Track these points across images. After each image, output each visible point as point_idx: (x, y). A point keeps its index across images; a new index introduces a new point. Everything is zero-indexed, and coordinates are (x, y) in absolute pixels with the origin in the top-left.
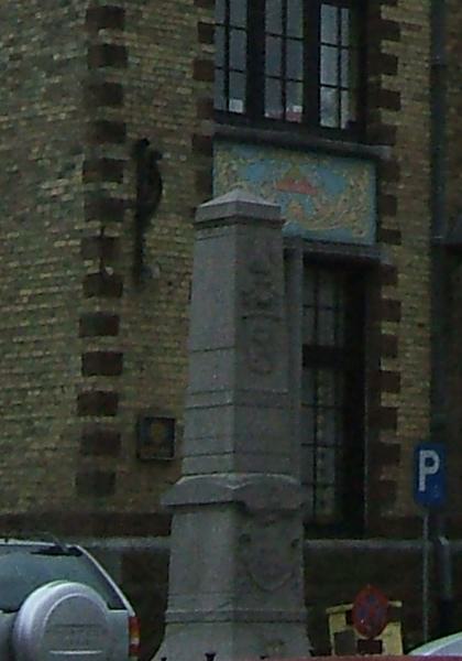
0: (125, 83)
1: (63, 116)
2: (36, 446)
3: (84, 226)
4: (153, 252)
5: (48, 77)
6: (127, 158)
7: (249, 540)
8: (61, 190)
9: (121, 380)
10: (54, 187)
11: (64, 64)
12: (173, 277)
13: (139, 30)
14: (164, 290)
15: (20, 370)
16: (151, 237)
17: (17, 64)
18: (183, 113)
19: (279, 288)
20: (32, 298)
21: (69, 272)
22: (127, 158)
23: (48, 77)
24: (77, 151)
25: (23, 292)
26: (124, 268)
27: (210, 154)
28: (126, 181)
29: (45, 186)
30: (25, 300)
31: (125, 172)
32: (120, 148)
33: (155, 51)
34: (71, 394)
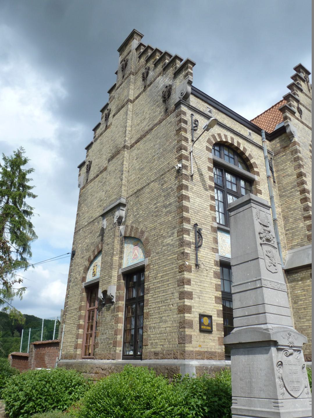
0: (189, 206)
1: (170, 219)
2: (164, 326)
3: (178, 250)
4: (201, 259)
5: (166, 209)
6: (191, 229)
7: (282, 364)
8: (170, 241)
9: (193, 301)
10: (168, 241)
11: (170, 204)
12: (208, 268)
13: (192, 192)
14: (206, 272)
15: (158, 300)
16: (200, 254)
17: (156, 209)
18: (207, 219)
19: (273, 233)
20: (162, 277)
21: (173, 266)
22: (191, 229)
23: (166, 209)
24: (174, 228)
25: (159, 275)
26: (192, 263)
27: (216, 232)
28: (191, 235)
29: (166, 240)
30: (160, 277)
31: (191, 233)
32: (189, 225)
33: (198, 200)
34: (175, 307)
